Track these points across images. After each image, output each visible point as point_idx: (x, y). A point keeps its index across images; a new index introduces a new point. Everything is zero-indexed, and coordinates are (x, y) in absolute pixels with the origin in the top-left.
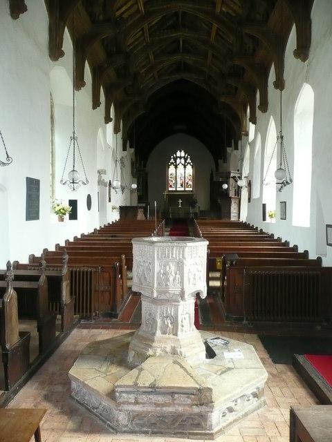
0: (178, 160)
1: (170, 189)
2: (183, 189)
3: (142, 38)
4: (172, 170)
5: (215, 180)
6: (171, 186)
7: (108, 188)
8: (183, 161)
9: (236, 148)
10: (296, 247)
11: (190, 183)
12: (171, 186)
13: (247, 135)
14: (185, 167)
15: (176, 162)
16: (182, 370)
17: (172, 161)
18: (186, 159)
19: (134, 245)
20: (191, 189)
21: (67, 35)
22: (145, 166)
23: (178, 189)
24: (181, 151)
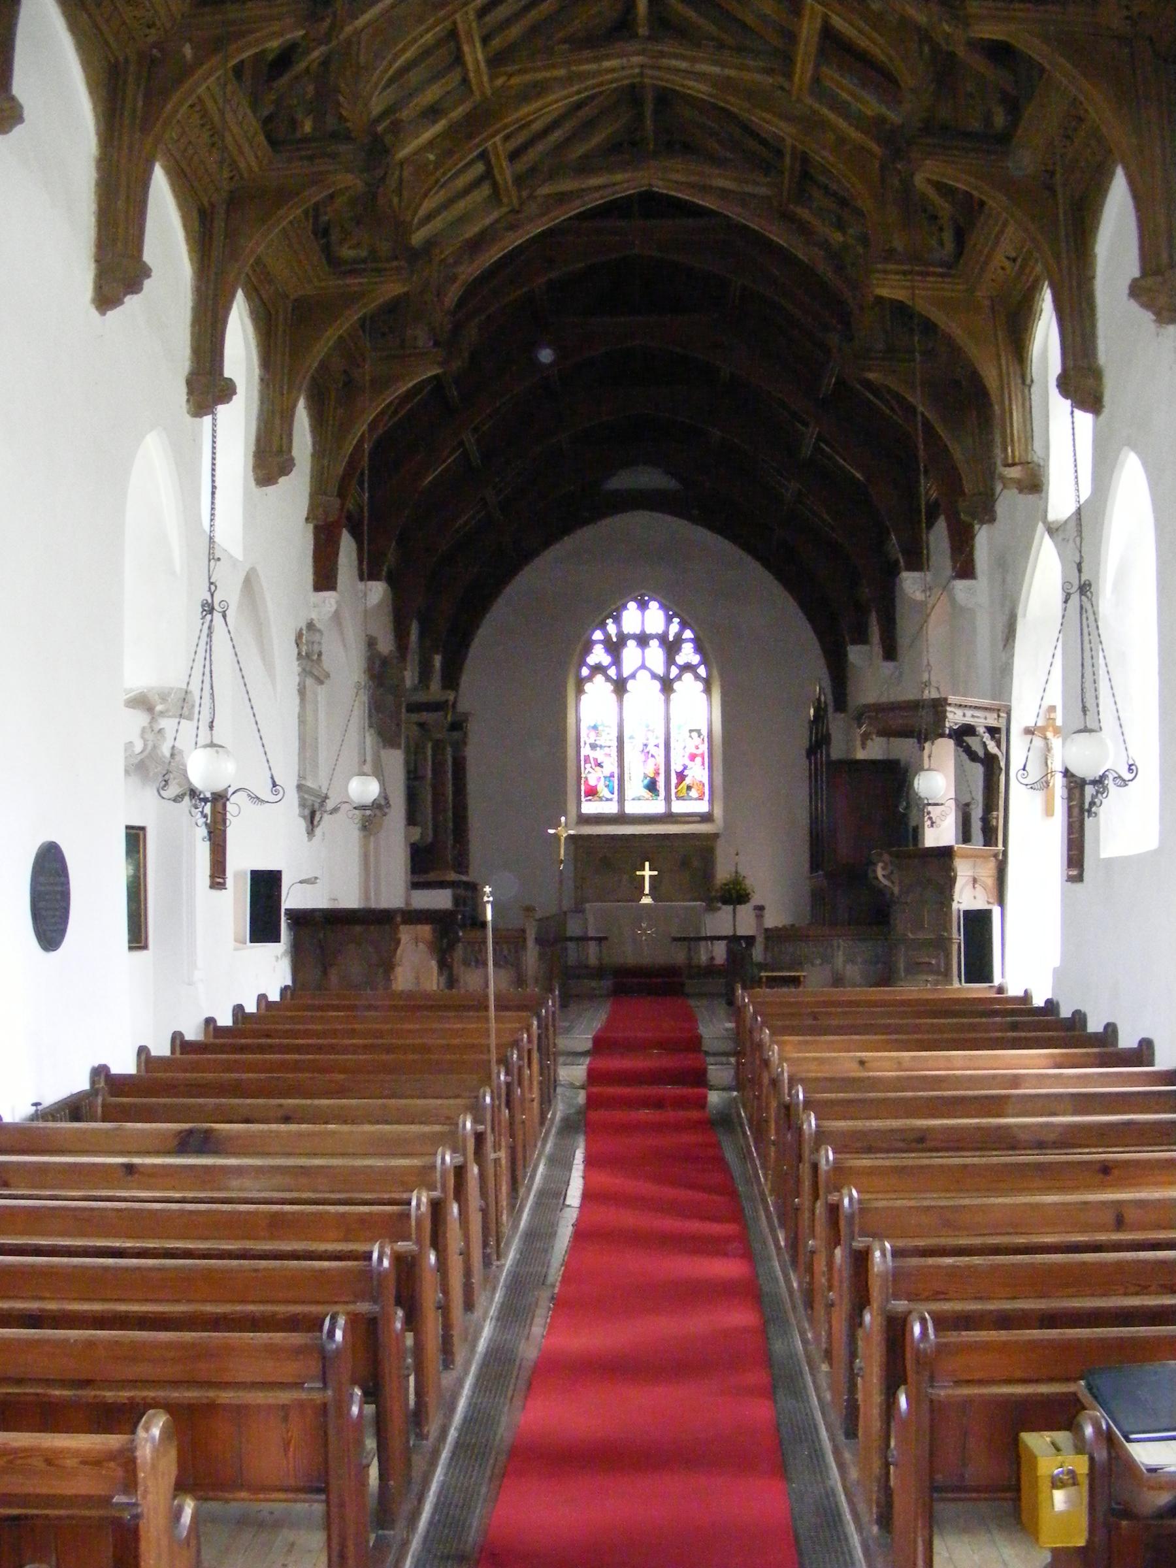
0: (631, 653)
2: (656, 807)
4: (597, 696)
5: (837, 751)
6: (592, 792)
8: (655, 655)
9: (890, 652)
10: (1027, 997)
11: (698, 773)
12: (592, 792)
13: (1034, 484)
14: (667, 685)
15: (617, 661)
16: (216, 484)
17: (598, 655)
18: (671, 648)
20: (702, 807)
21: (160, 184)
22: (451, 679)
23: (631, 808)
24: (643, 606)
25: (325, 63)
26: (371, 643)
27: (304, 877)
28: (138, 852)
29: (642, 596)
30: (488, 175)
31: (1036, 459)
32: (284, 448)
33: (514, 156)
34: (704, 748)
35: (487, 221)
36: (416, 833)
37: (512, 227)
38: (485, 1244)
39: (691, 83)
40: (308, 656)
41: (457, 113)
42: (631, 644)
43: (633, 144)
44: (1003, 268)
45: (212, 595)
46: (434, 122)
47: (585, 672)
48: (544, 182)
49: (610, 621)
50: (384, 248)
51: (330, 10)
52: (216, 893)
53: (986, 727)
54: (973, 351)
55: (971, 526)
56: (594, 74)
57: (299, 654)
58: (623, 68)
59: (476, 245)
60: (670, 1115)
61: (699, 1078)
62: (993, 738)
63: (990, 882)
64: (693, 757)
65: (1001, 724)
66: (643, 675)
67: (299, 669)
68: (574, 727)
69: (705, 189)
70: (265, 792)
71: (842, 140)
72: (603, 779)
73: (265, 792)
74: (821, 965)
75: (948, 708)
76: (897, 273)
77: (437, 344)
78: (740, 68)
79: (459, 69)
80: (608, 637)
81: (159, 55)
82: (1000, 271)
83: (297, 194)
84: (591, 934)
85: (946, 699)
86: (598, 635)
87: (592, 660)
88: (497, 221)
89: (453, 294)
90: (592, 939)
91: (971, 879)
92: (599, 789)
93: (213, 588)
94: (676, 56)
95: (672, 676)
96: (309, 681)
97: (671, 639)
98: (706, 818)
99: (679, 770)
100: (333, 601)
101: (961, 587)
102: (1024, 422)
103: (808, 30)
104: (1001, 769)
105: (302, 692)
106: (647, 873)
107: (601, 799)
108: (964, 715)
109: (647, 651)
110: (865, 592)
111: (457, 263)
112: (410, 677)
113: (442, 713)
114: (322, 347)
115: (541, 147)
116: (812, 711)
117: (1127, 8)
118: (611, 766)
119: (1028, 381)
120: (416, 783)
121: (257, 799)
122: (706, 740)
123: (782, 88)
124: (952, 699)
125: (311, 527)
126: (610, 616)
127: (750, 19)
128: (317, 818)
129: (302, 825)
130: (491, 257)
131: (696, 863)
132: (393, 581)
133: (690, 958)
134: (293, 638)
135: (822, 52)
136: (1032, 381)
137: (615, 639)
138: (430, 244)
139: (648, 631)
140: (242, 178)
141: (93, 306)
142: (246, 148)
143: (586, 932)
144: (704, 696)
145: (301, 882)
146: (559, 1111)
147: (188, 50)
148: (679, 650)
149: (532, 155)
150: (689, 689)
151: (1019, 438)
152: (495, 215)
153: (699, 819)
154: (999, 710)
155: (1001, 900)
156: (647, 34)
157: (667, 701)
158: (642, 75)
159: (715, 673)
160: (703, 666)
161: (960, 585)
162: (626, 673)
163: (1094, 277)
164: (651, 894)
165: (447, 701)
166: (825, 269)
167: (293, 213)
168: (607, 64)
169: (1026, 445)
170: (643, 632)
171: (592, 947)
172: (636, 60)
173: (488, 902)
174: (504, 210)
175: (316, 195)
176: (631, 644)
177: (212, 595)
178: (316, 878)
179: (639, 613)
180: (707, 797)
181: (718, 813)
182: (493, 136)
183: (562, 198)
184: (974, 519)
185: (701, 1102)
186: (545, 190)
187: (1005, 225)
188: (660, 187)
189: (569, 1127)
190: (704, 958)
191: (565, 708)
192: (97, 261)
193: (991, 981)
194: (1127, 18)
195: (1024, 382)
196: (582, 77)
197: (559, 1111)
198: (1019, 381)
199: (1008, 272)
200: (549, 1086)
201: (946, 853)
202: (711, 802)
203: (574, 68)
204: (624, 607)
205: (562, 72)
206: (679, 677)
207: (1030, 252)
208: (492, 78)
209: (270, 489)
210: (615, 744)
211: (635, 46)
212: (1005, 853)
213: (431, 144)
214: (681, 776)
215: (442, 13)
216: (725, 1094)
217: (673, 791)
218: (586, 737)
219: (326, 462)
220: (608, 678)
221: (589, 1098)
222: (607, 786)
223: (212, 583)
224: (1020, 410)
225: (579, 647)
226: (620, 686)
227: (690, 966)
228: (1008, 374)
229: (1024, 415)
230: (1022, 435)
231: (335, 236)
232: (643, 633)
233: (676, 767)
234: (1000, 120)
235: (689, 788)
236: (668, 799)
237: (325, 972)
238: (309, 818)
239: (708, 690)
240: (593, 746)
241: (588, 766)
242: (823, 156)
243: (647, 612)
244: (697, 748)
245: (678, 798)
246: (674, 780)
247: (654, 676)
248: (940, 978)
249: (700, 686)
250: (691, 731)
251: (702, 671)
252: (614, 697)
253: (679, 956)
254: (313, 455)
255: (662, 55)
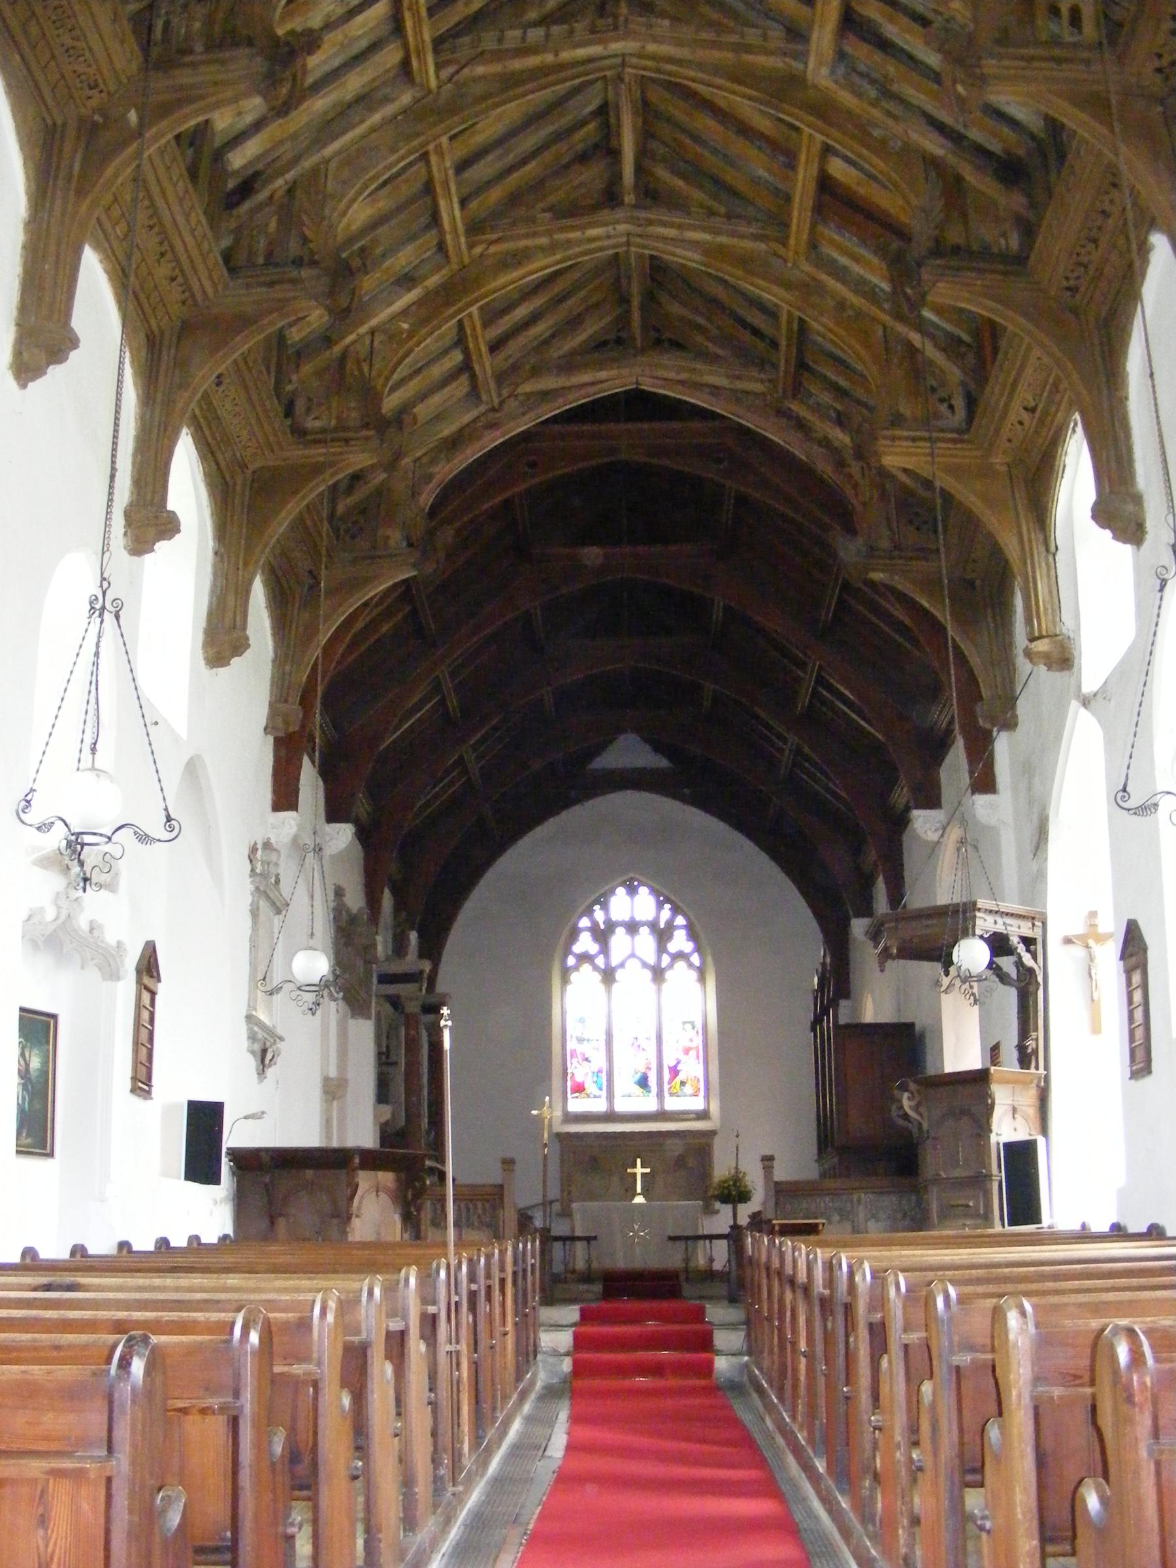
0: (620, 941)
1: (576, 1105)
2: (647, 1103)
3: (391, 56)
4: (585, 981)
6: (579, 1089)
7: (127, 987)
8: (646, 942)
11: (692, 1069)
12: (579, 1089)
14: (658, 974)
15: (605, 950)
16: (117, 466)
17: (585, 943)
18: (663, 935)
19: (707, 1311)
20: (698, 1104)
23: (621, 1106)
24: (632, 891)
25: (290, 191)
26: (339, 893)
27: (250, 1112)
28: (48, 1042)
29: (632, 880)
30: (466, 367)
31: (1064, 631)
32: (238, 623)
33: (494, 347)
34: (698, 1041)
35: (467, 418)
36: (386, 1111)
37: (492, 426)
38: (436, 1461)
39: (678, 251)
40: (264, 876)
41: (433, 281)
42: (620, 931)
43: (619, 341)
44: (1021, 423)
45: (104, 593)
46: (410, 290)
47: (571, 961)
48: (528, 379)
49: (597, 907)
50: (354, 417)
51: (288, 73)
52: (136, 1101)
53: (1021, 937)
54: (991, 521)
55: (991, 732)
56: (579, 242)
57: (253, 870)
58: (609, 237)
59: (454, 443)
60: (673, 1382)
61: (705, 1343)
62: (1028, 950)
63: (1032, 1112)
64: (687, 1051)
65: (1037, 933)
66: (633, 964)
67: (252, 888)
68: (559, 1017)
69: (699, 386)
70: (156, 828)
71: (842, 305)
72: (590, 1075)
73: (156, 828)
74: (839, 1222)
75: (978, 914)
76: (907, 438)
77: (410, 545)
78: (733, 234)
79: (434, 232)
80: (595, 925)
81: (101, 120)
82: (1019, 427)
83: (256, 322)
84: (578, 1233)
85: (975, 904)
86: (584, 922)
87: (578, 948)
88: (474, 421)
89: (427, 498)
90: (579, 1239)
91: (1011, 1108)
92: (586, 1086)
93: (105, 584)
94: (665, 224)
95: (664, 965)
96: (263, 904)
97: (662, 925)
98: (703, 1115)
99: (672, 1064)
100: (293, 823)
101: (981, 803)
102: (1050, 592)
103: (804, 181)
104: (1038, 984)
105: (255, 913)
106: (639, 1170)
107: (588, 1096)
108: (996, 922)
109: (637, 938)
110: (871, 855)
111: (433, 462)
112: (382, 945)
113: (417, 985)
114: (281, 525)
115: (522, 340)
116: (816, 980)
117: (1160, 56)
118: (599, 1061)
119: (1053, 549)
120: (390, 1069)
121: (144, 838)
122: (700, 1032)
123: (775, 254)
124: (981, 903)
125: (270, 739)
126: (597, 902)
127: (741, 185)
128: (269, 1056)
129: (252, 1063)
130: (467, 459)
131: (691, 1162)
132: (364, 835)
133: (687, 1260)
134: (246, 852)
135: (819, 210)
136: (1057, 548)
137: (602, 927)
138: (405, 409)
139: (637, 919)
140: (196, 304)
141: (10, 372)
142: (201, 267)
143: (573, 1230)
144: (698, 986)
145: (246, 1118)
146: (542, 1375)
147: (133, 116)
148: (670, 937)
149: (514, 348)
150: (682, 977)
151: (1046, 609)
152: (474, 413)
153: (693, 1116)
154: (1033, 918)
155: (1044, 1130)
156: (634, 202)
157: (659, 991)
158: (628, 244)
159: (709, 959)
160: (696, 954)
161: (981, 800)
162: (614, 962)
163: (1127, 398)
164: (645, 1193)
165: (421, 972)
166: (825, 468)
167: (247, 343)
168: (592, 232)
169: (1054, 617)
170: (632, 919)
171: (580, 1246)
172: (622, 228)
173: (446, 1026)
174: (483, 408)
175: (273, 323)
176: (620, 931)
177: (104, 593)
178: (263, 1113)
179: (628, 898)
180: (702, 1093)
181: (715, 1108)
182: (471, 304)
183: (545, 396)
184: (994, 726)
185: (710, 1365)
186: (527, 388)
187: (1029, 349)
188: (647, 386)
189: (551, 1393)
190: (701, 1261)
191: (550, 997)
192: (18, 325)
193: (1039, 1221)
194: (1159, 70)
195: (1048, 550)
196: (569, 243)
197: (542, 1375)
198: (1042, 549)
199: (1027, 423)
200: (527, 1352)
201: (978, 1080)
202: (707, 1097)
203: (556, 237)
204: (612, 892)
205: (544, 241)
206: (671, 966)
207: (1057, 379)
208: (471, 246)
209: (221, 671)
210: (603, 1037)
211: (620, 214)
212: (1047, 1079)
213: (405, 313)
214: (674, 1072)
215: (415, 143)
216: (734, 1360)
217: (666, 1087)
218: (572, 1030)
219: (288, 668)
220: (596, 968)
221: (575, 1363)
222: (596, 1082)
223: (104, 579)
224: (1045, 579)
225: (566, 931)
226: (608, 976)
227: (686, 1270)
228: (1030, 541)
229: (1049, 586)
230: (1049, 606)
231: (300, 405)
232: (632, 920)
233: (669, 1061)
234: (1014, 242)
235: (683, 1083)
236: (660, 1095)
237: (272, 1223)
238: (259, 1054)
239: (702, 979)
240: (580, 1040)
241: (574, 1061)
242: (821, 326)
243: (637, 898)
244: (691, 1040)
245: (671, 1095)
246: (666, 1076)
247: (645, 965)
248: (979, 1221)
249: (694, 975)
250: (684, 1023)
251: (695, 959)
252: (601, 987)
253: (673, 1259)
254: (274, 661)
255: (651, 222)
